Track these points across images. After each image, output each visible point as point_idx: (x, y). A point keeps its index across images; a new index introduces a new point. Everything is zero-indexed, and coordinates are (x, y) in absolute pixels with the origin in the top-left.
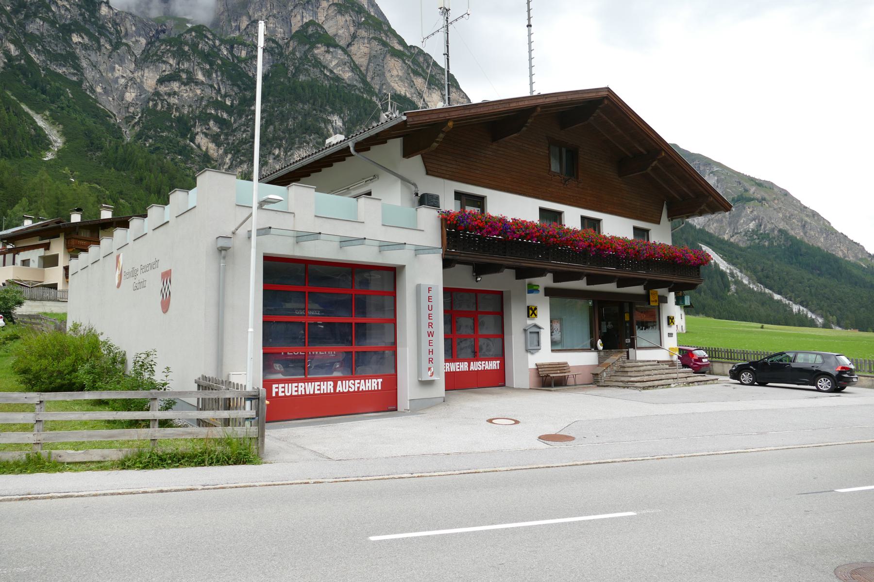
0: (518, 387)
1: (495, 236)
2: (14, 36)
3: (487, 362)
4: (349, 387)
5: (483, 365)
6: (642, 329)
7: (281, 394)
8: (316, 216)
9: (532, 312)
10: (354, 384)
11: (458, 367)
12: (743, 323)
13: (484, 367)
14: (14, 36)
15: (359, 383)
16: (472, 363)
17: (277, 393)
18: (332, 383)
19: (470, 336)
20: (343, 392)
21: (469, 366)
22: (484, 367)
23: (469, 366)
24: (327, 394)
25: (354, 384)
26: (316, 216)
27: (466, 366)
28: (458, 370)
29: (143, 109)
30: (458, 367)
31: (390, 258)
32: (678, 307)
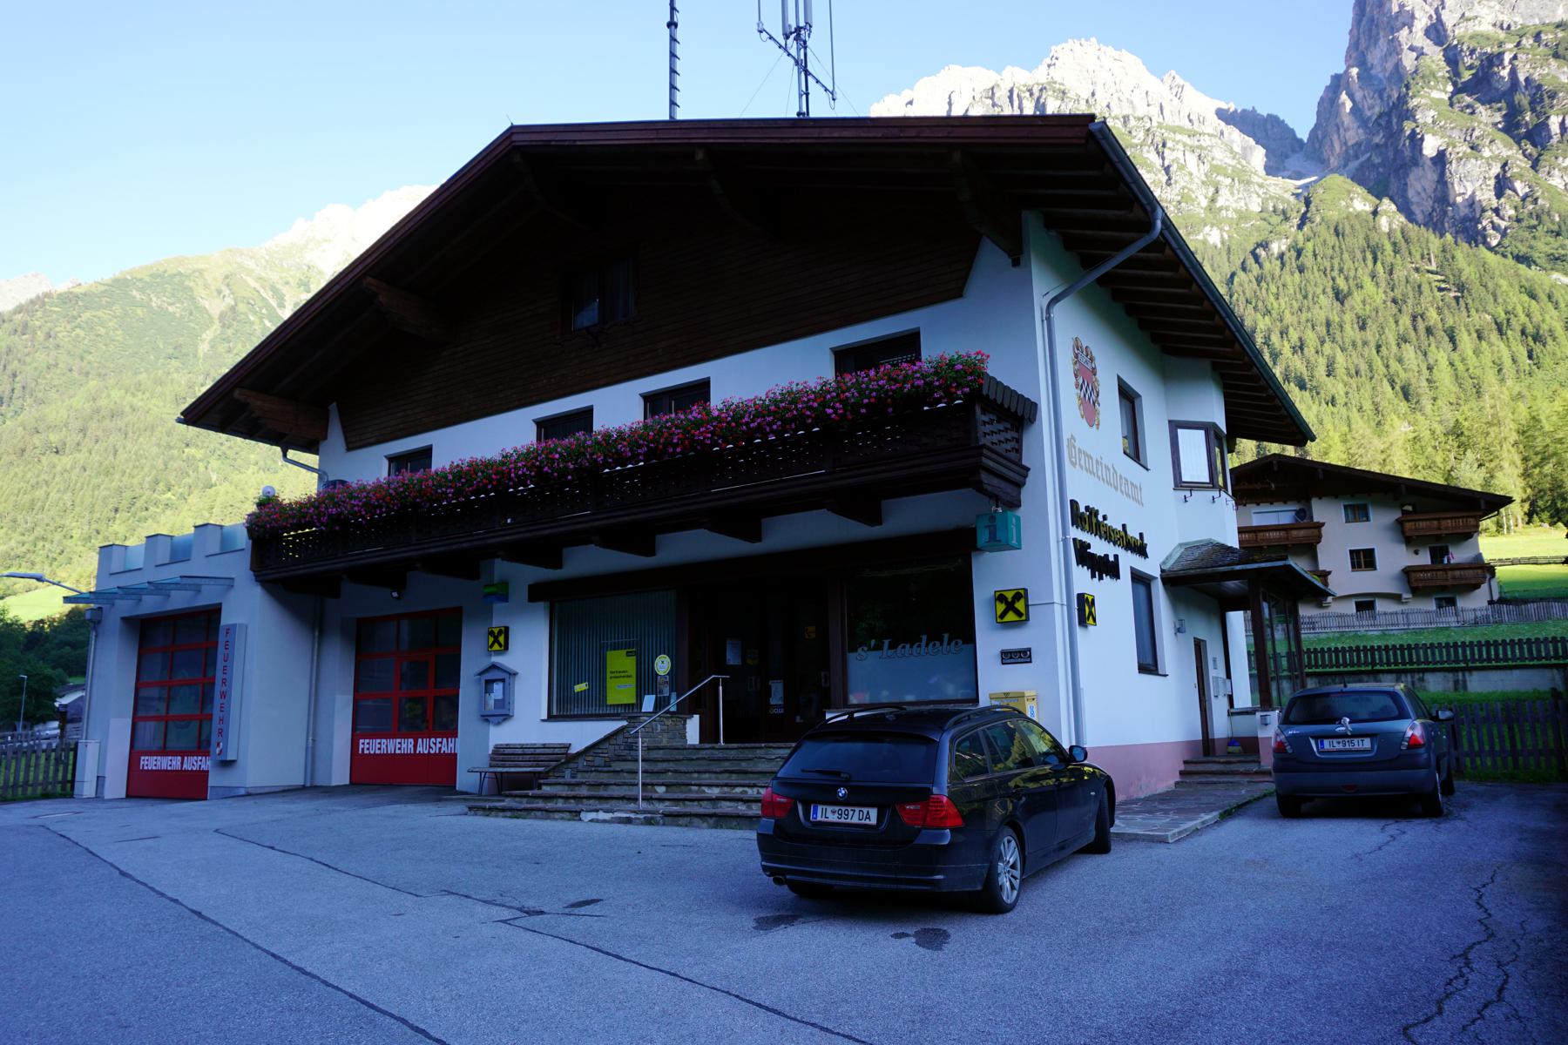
0: (464, 790)
1: (618, 468)
2: (76, 482)
3: (445, 740)
4: (430, 747)
5: (438, 745)
6: (879, 647)
7: (366, 752)
8: (157, 566)
9: (501, 641)
10: (435, 744)
11: (398, 746)
12: (334, 768)
13: (440, 749)
14: (76, 482)
15: (441, 743)
16: (420, 740)
17: (363, 749)
18: (179, 758)
19: (190, 718)
20: (424, 754)
21: (415, 746)
22: (440, 749)
23: (415, 746)
24: (407, 754)
25: (435, 744)
26: (157, 566)
27: (411, 746)
28: (398, 752)
29: (1540, 493)
30: (398, 746)
31: (205, 599)
32: (1420, 45)
